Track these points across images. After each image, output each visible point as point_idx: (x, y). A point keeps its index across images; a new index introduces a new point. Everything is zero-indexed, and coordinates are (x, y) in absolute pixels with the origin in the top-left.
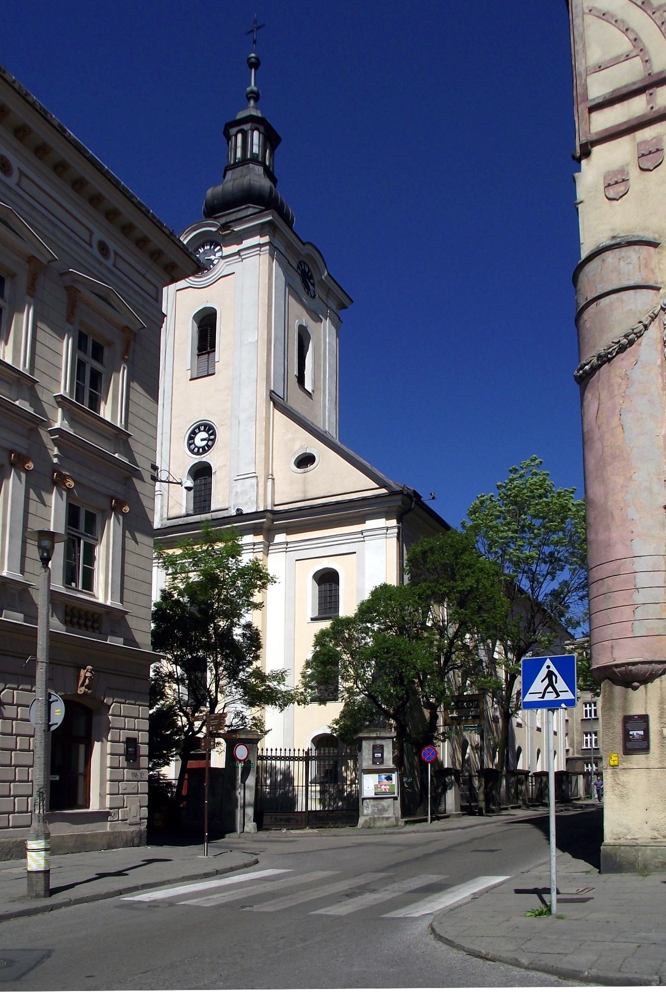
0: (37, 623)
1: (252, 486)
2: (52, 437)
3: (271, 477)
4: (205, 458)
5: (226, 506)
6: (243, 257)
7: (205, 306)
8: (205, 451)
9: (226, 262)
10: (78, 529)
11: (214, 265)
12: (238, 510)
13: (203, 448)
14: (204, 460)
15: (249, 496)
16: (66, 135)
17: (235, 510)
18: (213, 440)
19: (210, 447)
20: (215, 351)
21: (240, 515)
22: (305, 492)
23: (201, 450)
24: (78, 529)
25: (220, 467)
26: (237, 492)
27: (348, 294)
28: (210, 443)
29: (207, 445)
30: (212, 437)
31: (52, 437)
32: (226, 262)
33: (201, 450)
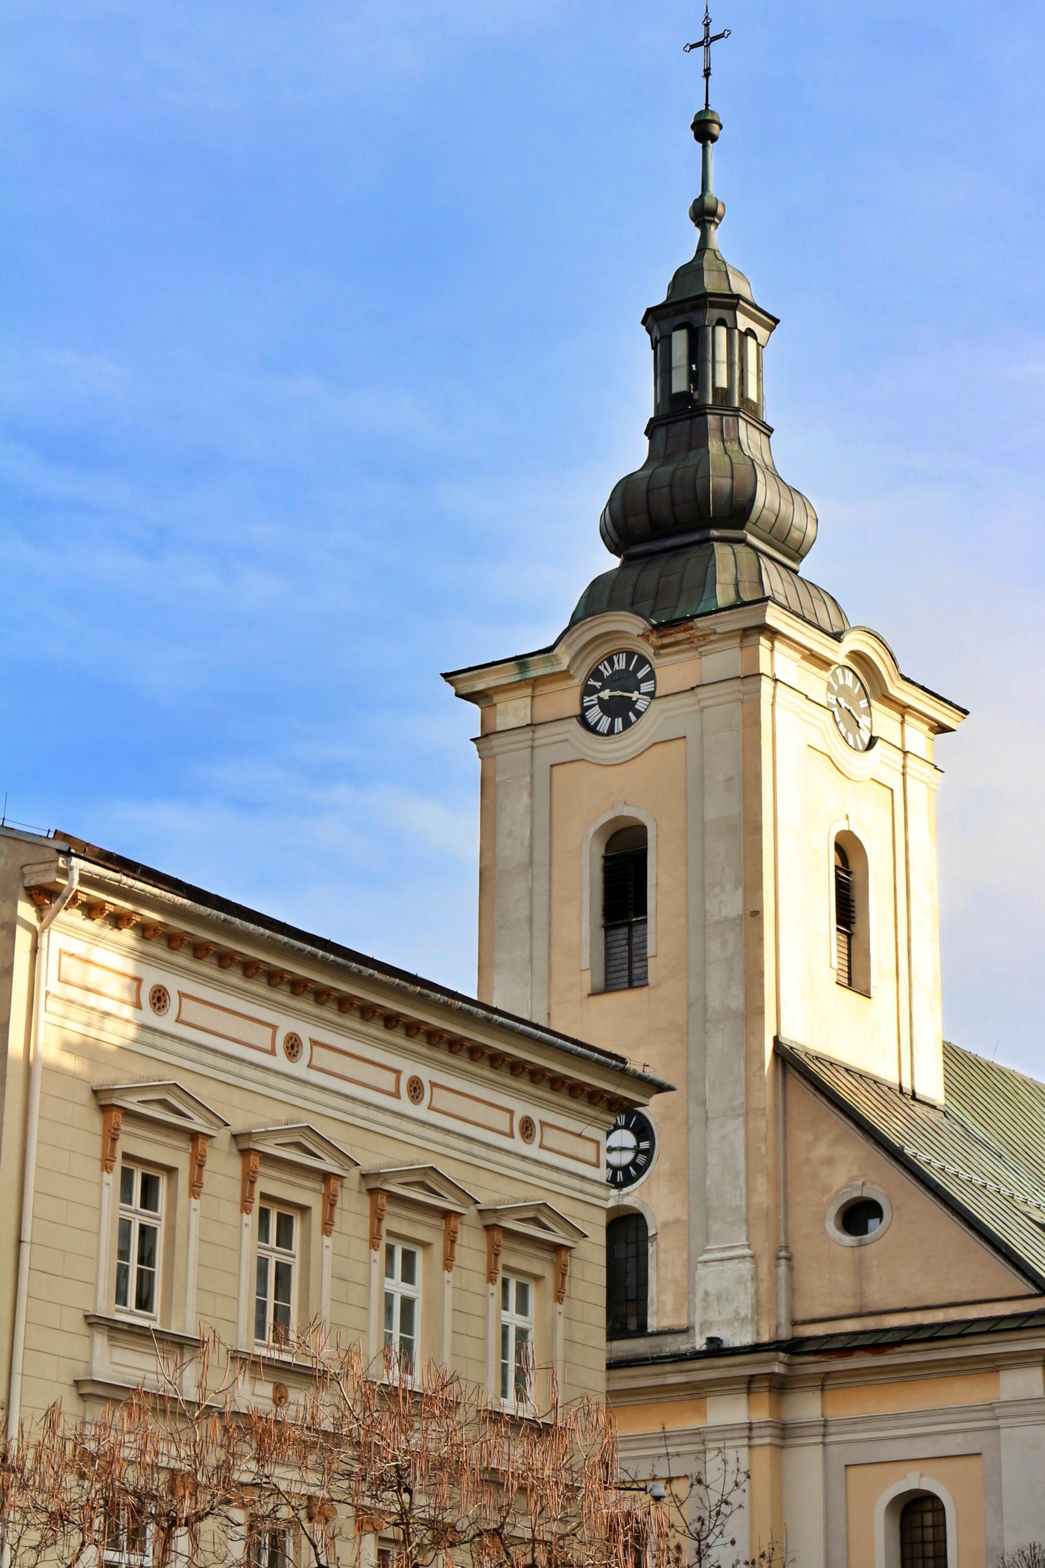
0: (118, 1267)
1: (740, 1280)
2: (288, 1305)
3: (783, 1254)
4: (631, 1197)
5: (682, 1322)
6: (703, 704)
7: (618, 814)
8: (629, 1180)
9: (663, 711)
10: (290, 1249)
11: (639, 714)
12: (711, 1340)
13: (625, 1169)
14: (627, 1201)
15: (735, 1304)
16: (432, 1001)
17: (705, 1341)
18: (649, 1153)
19: (641, 1170)
20: (645, 921)
21: (716, 1349)
22: (860, 1292)
23: (620, 1174)
24: (290, 1249)
25: (666, 1225)
26: (707, 1293)
27: (994, 1226)
28: (641, 1160)
29: (633, 1163)
30: (644, 1145)
31: (288, 1305)
32: (663, 711)
33: (620, 1174)
